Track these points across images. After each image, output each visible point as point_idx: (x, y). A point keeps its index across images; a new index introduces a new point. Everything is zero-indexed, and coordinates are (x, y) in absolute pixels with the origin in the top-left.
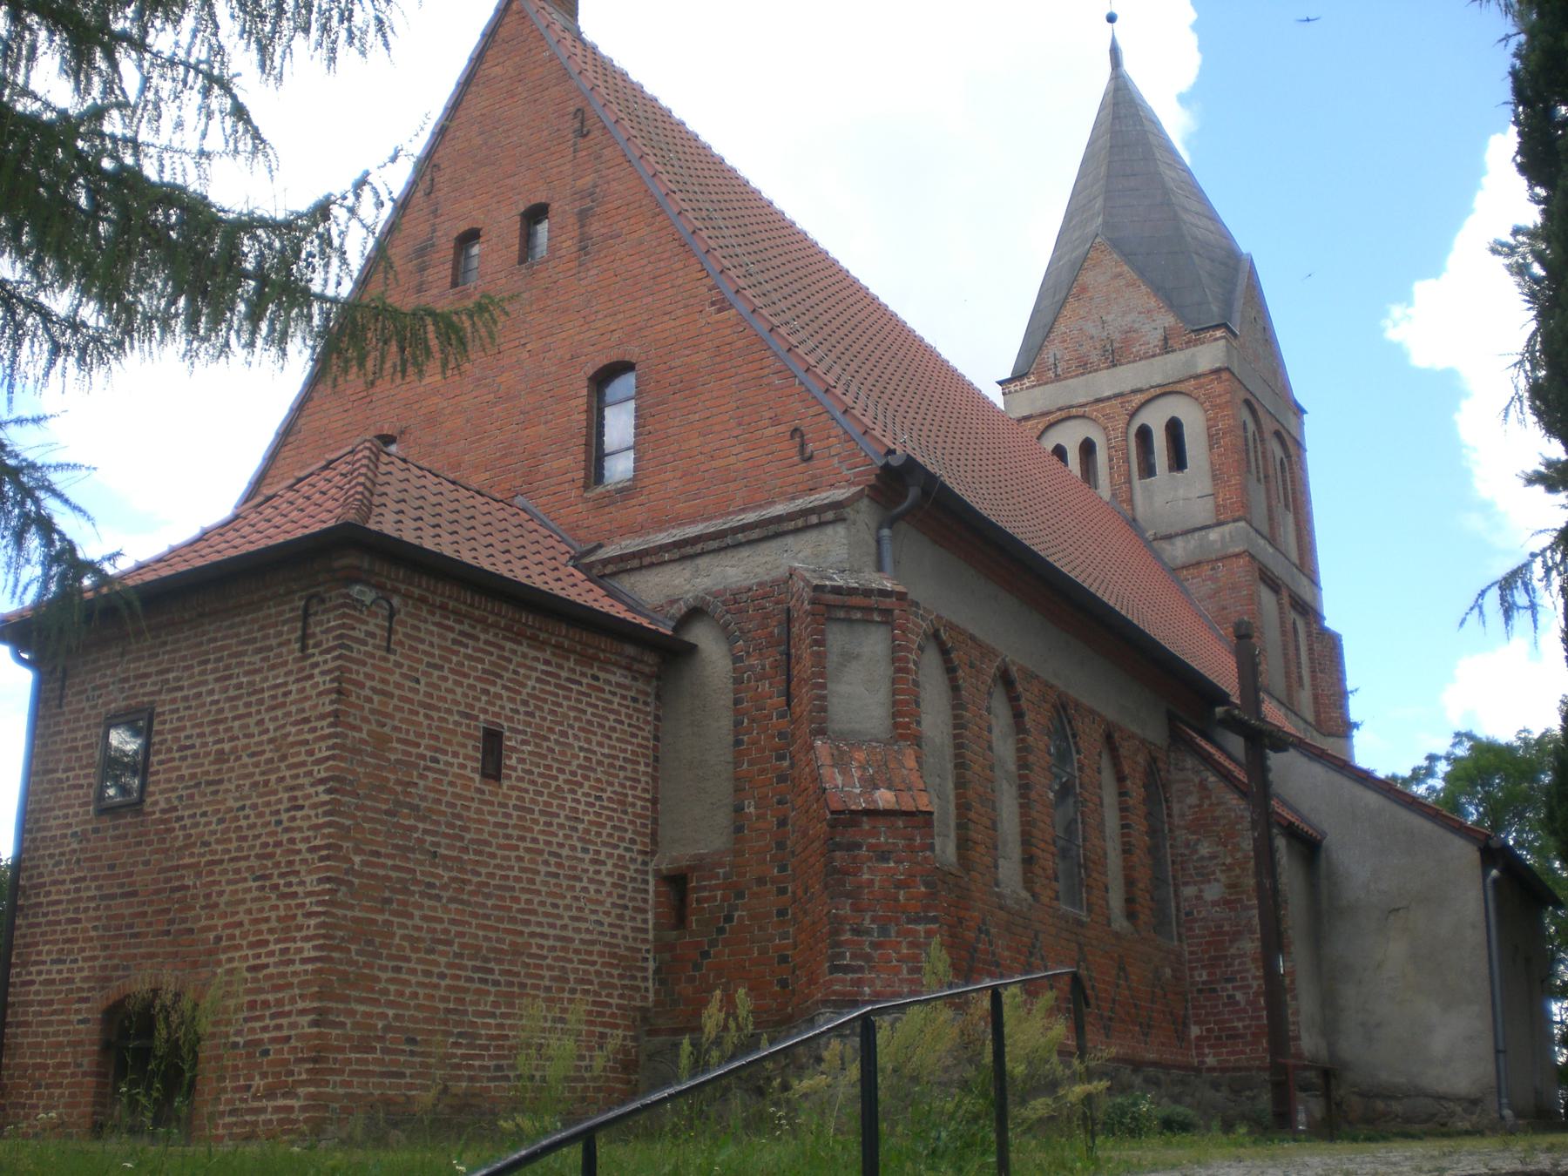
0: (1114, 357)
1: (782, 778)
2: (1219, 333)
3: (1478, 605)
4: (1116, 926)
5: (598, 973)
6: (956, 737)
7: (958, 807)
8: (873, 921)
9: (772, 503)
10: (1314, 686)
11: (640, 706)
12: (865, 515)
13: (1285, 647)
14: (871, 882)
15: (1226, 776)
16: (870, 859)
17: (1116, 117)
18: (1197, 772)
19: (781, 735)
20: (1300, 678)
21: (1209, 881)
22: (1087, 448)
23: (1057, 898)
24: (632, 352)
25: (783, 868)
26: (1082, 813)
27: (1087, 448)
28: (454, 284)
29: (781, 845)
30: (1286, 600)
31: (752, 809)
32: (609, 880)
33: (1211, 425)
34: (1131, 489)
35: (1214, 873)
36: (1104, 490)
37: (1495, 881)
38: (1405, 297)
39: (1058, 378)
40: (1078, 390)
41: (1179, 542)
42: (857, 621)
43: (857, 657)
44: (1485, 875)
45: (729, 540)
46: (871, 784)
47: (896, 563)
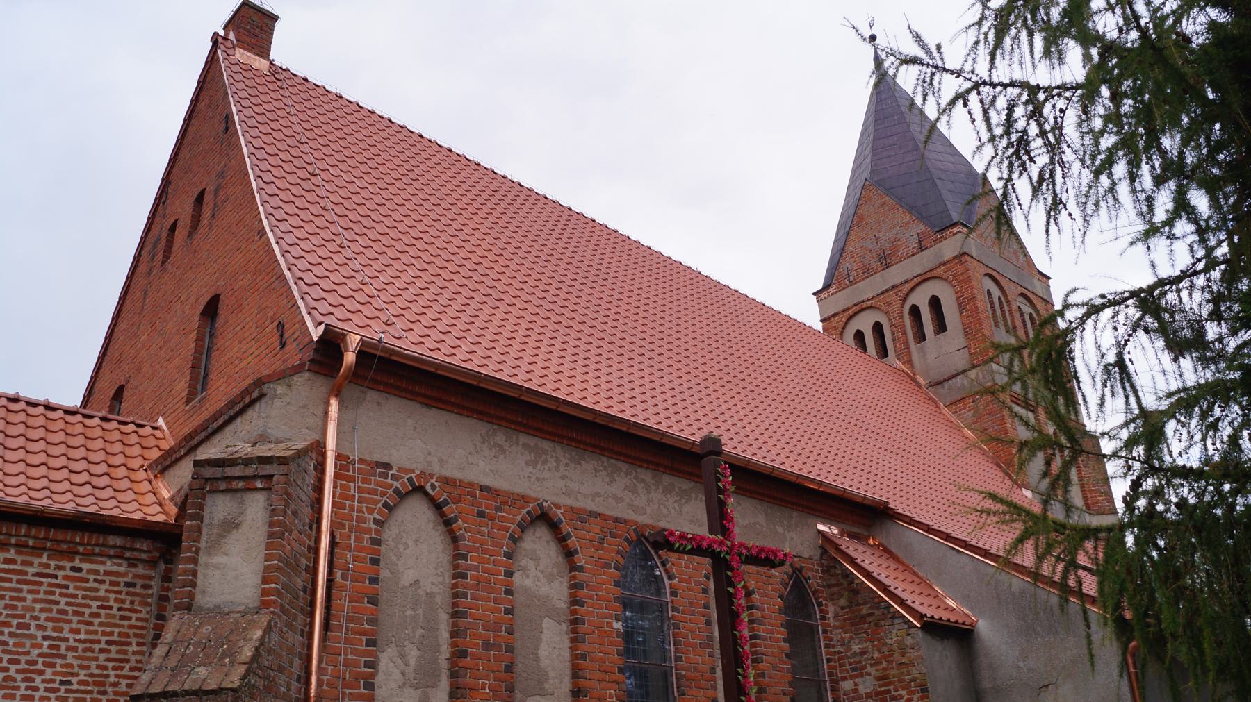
0: (886, 261)
11: (138, 590)
22: (878, 328)
27: (878, 328)
34: (909, 353)
40: (867, 289)
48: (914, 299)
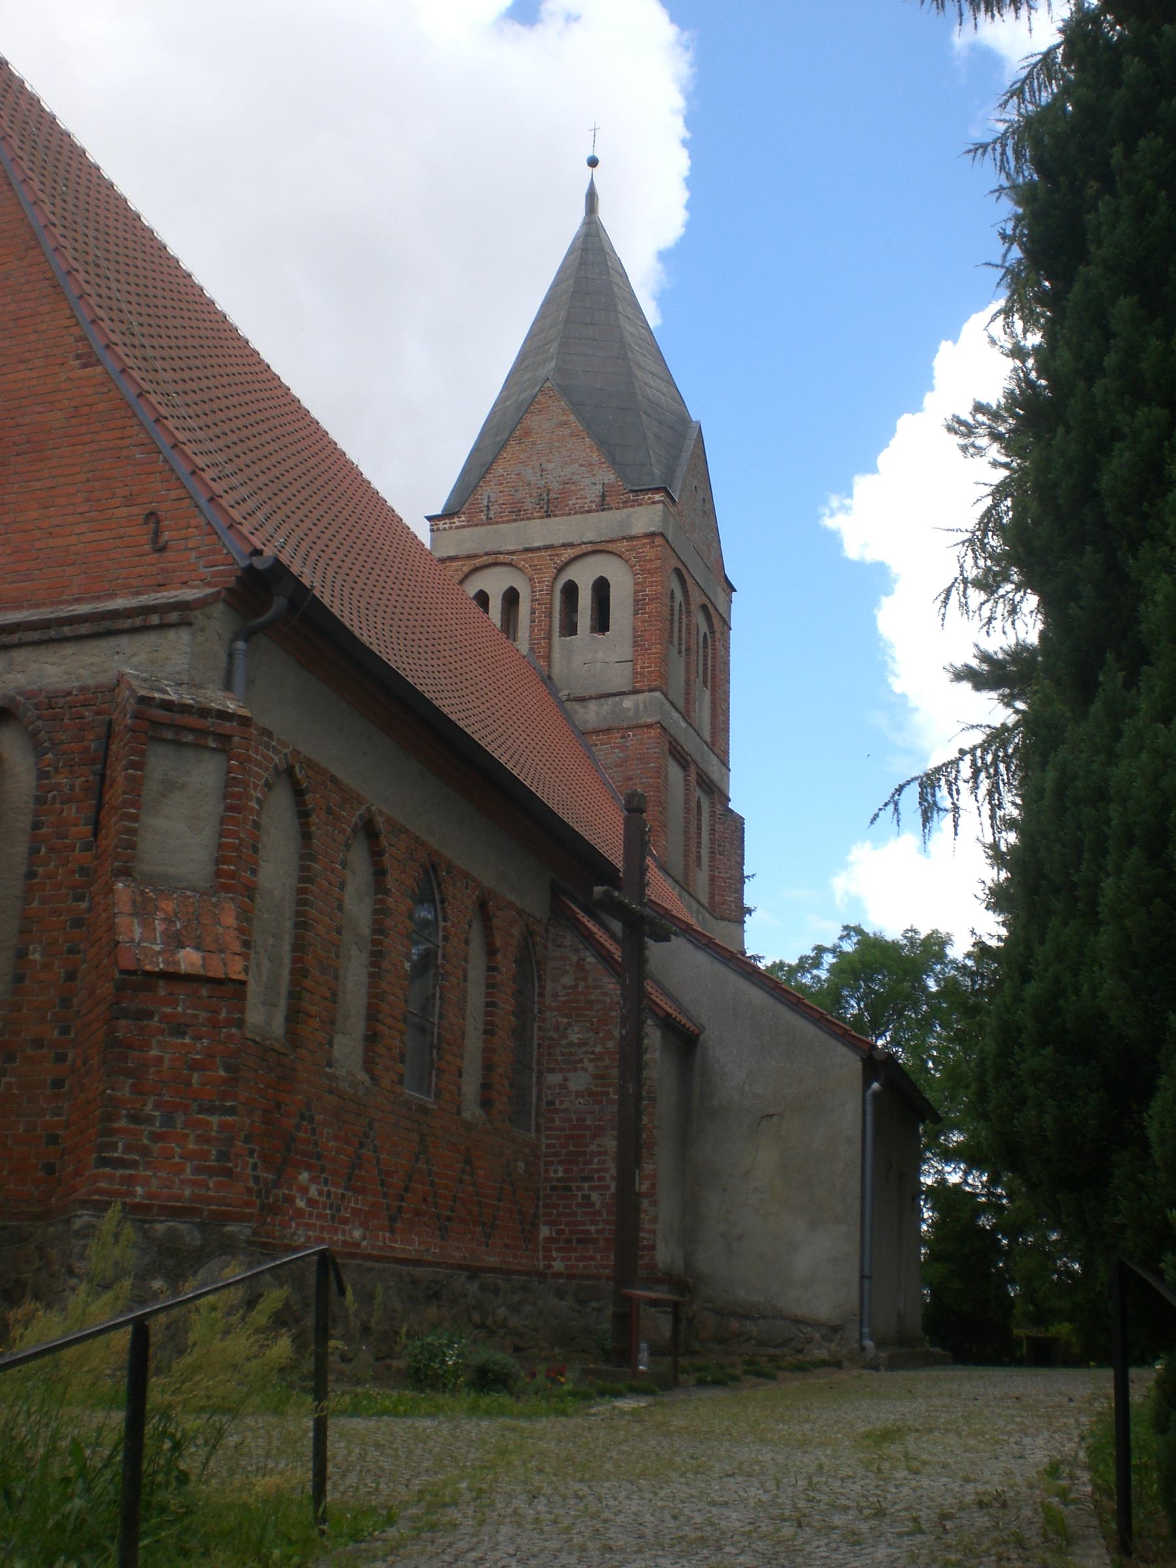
0: (549, 507)
1: (77, 923)
2: (657, 497)
3: (894, 802)
4: (467, 1115)
6: (300, 891)
7: (293, 972)
8: (157, 1106)
9: (112, 596)
10: (712, 868)
12: (218, 623)
13: (687, 823)
14: (159, 1060)
15: (605, 957)
16: (162, 1032)
17: (583, 263)
18: (577, 951)
19: (84, 871)
20: (699, 857)
21: (575, 1069)
22: (511, 597)
23: (401, 1082)
25: (65, 1031)
26: (442, 987)
27: (511, 597)
29: (66, 1002)
30: (693, 777)
31: (37, 956)
33: (639, 588)
34: (550, 647)
35: (581, 1061)
36: (523, 643)
37: (876, 1095)
38: (847, 490)
39: (489, 521)
41: (592, 706)
42: (186, 744)
43: (183, 787)
44: (866, 1085)
45: (52, 633)
46: (176, 941)
47: (250, 682)
48: (570, 574)
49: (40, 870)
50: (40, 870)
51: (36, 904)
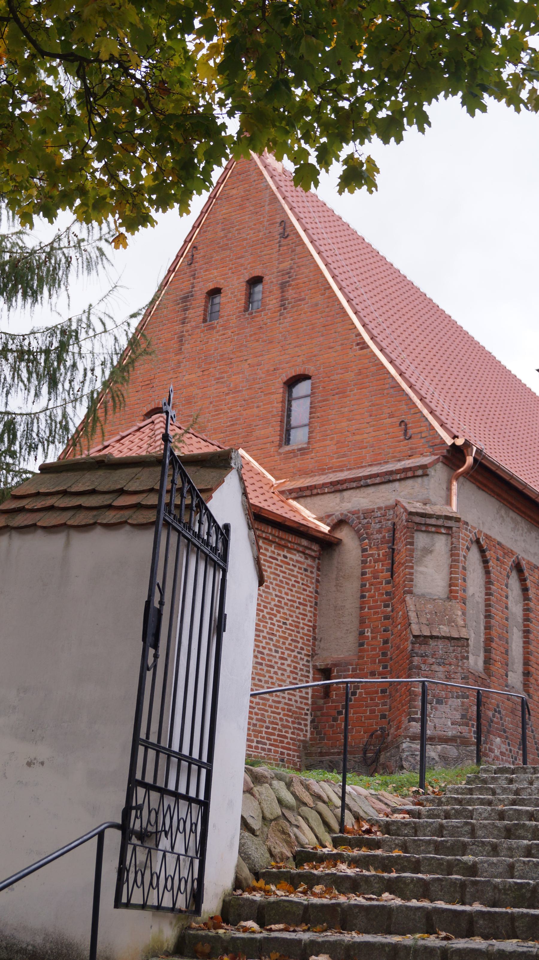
1: (387, 618)
5: (281, 719)
6: (486, 600)
19: (388, 594)
24: (310, 369)
25: (385, 667)
28: (205, 321)
29: (384, 654)
31: (369, 634)
32: (288, 669)
49: (367, 594)
50: (367, 594)
51: (366, 610)
